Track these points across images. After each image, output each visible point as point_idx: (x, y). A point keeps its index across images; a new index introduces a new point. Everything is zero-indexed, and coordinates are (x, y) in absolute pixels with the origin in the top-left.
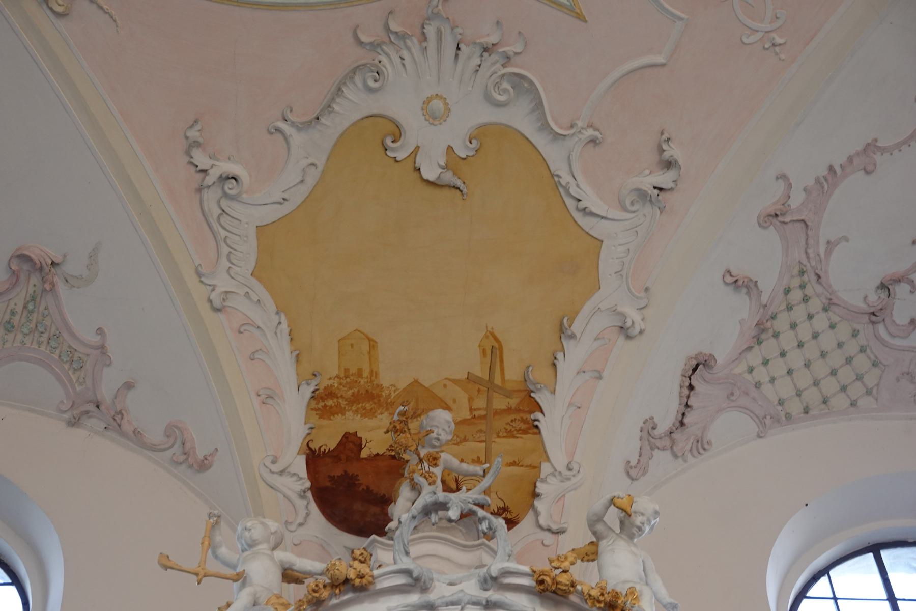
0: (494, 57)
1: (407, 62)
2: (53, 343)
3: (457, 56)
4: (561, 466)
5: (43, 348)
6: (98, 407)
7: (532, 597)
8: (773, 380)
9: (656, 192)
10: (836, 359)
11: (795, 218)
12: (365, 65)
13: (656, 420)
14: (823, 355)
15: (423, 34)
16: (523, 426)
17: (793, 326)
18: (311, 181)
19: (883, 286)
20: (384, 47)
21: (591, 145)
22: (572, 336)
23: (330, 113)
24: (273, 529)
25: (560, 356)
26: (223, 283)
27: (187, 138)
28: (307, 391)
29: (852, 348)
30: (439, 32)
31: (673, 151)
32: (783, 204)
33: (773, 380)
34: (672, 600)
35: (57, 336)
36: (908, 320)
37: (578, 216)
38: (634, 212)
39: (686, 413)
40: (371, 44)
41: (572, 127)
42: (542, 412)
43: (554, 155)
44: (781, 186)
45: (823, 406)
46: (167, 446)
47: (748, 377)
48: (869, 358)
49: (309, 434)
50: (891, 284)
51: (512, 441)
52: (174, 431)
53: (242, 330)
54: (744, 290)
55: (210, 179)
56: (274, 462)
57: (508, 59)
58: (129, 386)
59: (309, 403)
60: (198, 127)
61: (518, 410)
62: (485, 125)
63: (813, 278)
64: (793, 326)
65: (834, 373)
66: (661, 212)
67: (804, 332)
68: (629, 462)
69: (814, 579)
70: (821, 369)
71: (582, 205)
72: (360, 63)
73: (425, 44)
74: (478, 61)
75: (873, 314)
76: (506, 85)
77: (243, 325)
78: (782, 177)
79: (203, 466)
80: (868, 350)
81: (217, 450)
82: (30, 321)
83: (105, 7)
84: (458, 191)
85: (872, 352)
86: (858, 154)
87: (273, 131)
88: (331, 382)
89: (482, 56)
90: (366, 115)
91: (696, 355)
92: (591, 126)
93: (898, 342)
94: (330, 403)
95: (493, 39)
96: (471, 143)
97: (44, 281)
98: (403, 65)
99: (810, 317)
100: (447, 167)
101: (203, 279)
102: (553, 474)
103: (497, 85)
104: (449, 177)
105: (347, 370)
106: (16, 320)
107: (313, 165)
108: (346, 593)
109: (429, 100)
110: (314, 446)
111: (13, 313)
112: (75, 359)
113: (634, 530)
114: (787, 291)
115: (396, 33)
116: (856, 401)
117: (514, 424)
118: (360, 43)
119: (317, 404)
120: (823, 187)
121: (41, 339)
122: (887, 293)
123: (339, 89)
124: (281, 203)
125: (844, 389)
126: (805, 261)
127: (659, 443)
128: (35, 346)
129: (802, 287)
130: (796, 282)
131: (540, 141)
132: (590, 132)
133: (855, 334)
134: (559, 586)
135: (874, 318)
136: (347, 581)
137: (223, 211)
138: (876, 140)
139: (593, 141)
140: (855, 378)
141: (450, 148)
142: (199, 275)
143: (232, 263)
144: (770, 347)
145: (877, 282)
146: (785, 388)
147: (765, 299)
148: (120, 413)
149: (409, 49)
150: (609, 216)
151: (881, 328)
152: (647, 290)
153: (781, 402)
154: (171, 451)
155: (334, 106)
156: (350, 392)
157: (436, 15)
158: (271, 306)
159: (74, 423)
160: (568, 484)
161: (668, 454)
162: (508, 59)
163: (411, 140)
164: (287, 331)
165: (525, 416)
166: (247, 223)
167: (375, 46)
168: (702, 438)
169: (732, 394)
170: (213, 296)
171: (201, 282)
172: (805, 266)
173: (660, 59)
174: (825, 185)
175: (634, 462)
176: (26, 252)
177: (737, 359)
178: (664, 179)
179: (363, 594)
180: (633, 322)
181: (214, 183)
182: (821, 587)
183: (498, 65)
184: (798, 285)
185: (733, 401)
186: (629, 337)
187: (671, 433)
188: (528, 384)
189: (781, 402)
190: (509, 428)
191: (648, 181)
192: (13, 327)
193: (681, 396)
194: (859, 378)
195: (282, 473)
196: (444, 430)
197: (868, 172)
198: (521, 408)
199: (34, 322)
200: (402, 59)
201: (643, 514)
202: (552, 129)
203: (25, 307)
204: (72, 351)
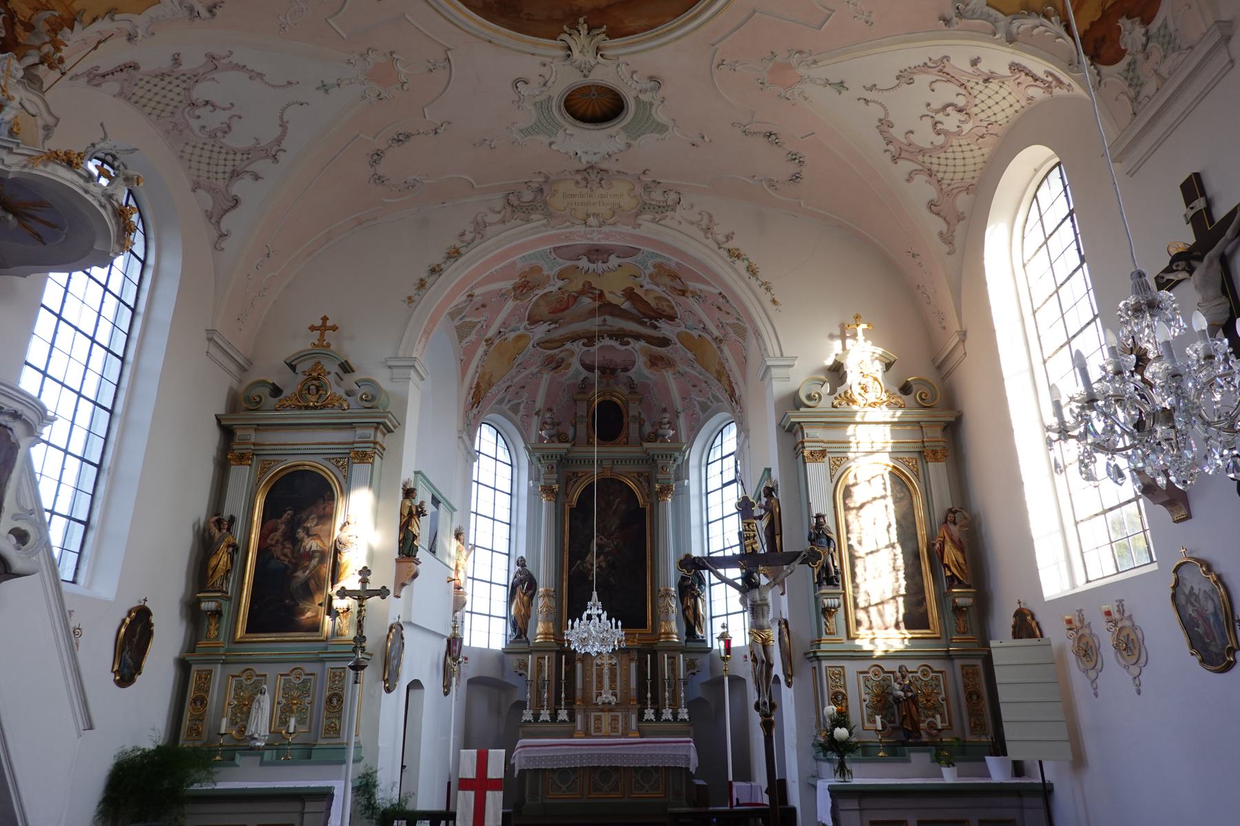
93: (187, 116)
114: (183, 75)
146: (141, 93)
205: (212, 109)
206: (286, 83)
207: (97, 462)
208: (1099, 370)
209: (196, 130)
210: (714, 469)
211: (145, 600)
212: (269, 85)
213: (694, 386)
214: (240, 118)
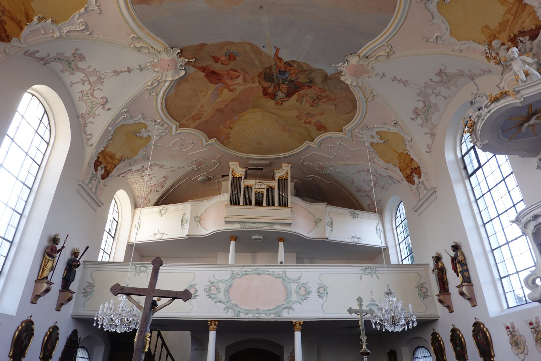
16: (524, 6)
18: (446, 21)
26: (457, 48)
51: (525, 11)
88: (488, 40)
107: (442, 20)
111: (447, 79)
136: (472, 126)
156: (492, 38)
165: (522, 4)
190: (521, 10)
207: (21, 213)
208: (365, 275)
210: (464, 146)
211: (31, 316)
213: (479, 110)
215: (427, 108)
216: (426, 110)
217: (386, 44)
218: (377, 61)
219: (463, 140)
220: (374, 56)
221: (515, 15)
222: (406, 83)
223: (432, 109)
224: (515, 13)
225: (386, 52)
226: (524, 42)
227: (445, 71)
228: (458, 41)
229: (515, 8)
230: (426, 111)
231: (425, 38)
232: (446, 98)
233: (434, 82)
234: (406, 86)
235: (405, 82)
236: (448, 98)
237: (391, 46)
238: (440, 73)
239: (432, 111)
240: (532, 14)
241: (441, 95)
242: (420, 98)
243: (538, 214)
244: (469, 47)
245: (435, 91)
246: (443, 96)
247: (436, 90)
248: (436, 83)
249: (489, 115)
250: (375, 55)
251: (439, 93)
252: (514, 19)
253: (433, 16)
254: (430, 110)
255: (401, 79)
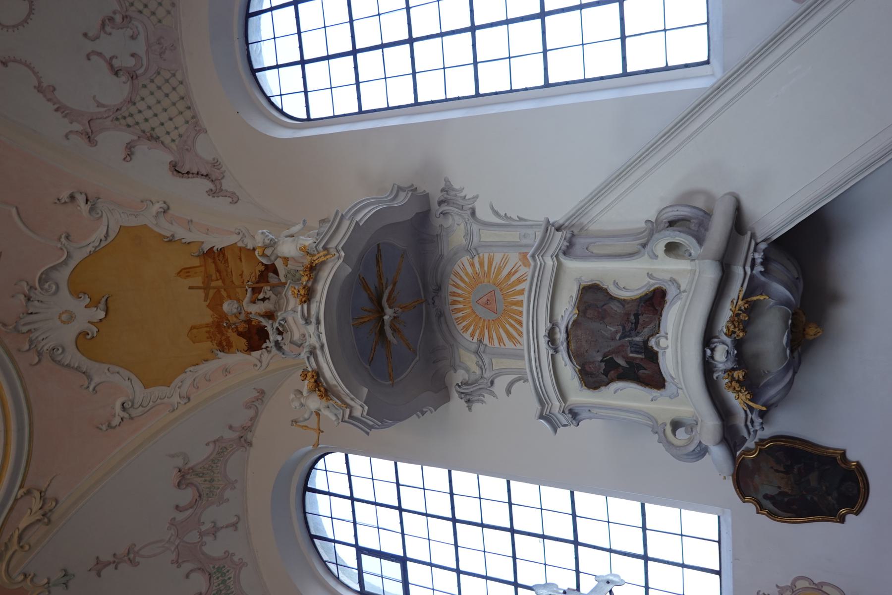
0: (32, 294)
1: (44, 337)
2: (216, 461)
3: (36, 313)
4: (239, 237)
5: (219, 465)
6: (242, 437)
7: (311, 302)
8: (176, 128)
9: (89, 203)
10: (159, 95)
11: (88, 126)
12: (51, 357)
13: (208, 189)
14: (159, 102)
15: (27, 332)
16: (221, 255)
17: (146, 120)
18: (117, 369)
19: (116, 74)
20: (39, 349)
21: (69, 238)
22: (173, 236)
23: (80, 367)
24: (294, 396)
25: (184, 241)
26: (176, 399)
27: (107, 430)
28: (221, 354)
29: (152, 87)
30: (24, 325)
31: (64, 196)
32: (82, 134)
33: (176, 128)
34: (302, 223)
35: (213, 460)
36: (132, 58)
37: (110, 240)
38: (102, 212)
39: (201, 174)
40: (38, 356)
41: (62, 249)
42: (214, 247)
43: (78, 257)
44: (71, 136)
45: (185, 99)
46: (255, 407)
47: (177, 141)
48: (156, 77)
49: (241, 351)
50: (114, 70)
51: (229, 260)
52: (248, 406)
53: (197, 387)
54: (132, 149)
55: (125, 415)
56: (256, 366)
57: (32, 288)
58: (231, 427)
59: (226, 353)
60: (100, 426)
61: (214, 258)
62: (70, 292)
63: (119, 112)
64: (146, 120)
65: (167, 95)
66: (99, 198)
67: (149, 114)
68: (231, 202)
69: (272, 104)
70: (166, 102)
71: (103, 238)
72: (50, 359)
73: (33, 330)
74: (36, 302)
75: (132, 78)
76: (46, 286)
77: (194, 386)
78: (67, 136)
79: (262, 392)
80: (152, 78)
81: (254, 388)
82: (208, 473)
83: (48, 483)
84: (108, 299)
85: (153, 75)
86: (45, 96)
87: (95, 392)
89: (33, 301)
90: (77, 351)
91: (171, 171)
92: (59, 239)
93: (145, 62)
94: (224, 344)
95: (22, 297)
96: (81, 297)
97: (188, 473)
98: (46, 338)
99: (140, 112)
100: (97, 307)
101: (175, 408)
102: (243, 241)
103: (47, 291)
104: (102, 305)
105: (208, 338)
106: (208, 479)
107: (108, 370)
108: (320, 380)
109: (62, 322)
110: (246, 348)
111: (205, 481)
112: (222, 451)
113: (272, 242)
114: (129, 126)
115: (30, 346)
116: (179, 82)
117: (221, 260)
118: (40, 361)
119: (226, 349)
120: (68, 113)
121: (215, 466)
122: (120, 71)
123: (67, 365)
124: (131, 381)
125: (174, 89)
126: (110, 118)
127: (218, 187)
128: (219, 468)
129: (125, 118)
130: (123, 121)
131: (72, 264)
132: (63, 240)
133: (145, 86)
134: (306, 293)
135: (134, 77)
136: (316, 381)
137: (140, 406)
138: (35, 87)
139: (67, 237)
140: (167, 84)
141: (86, 307)
142: (174, 410)
143: (165, 397)
144: (159, 132)
145: (115, 77)
146: (179, 120)
147: (135, 138)
148: (243, 428)
149: (37, 337)
150: (107, 224)
151: (139, 72)
152: (142, 202)
153: (187, 122)
154: (258, 406)
155: (76, 366)
156: (218, 335)
157: (16, 329)
158: (184, 375)
159: (250, 444)
160: (246, 234)
161: (223, 181)
162: (32, 288)
163: (86, 326)
164: (193, 367)
165: (216, 255)
166: (144, 394)
167: (40, 354)
168: (212, 163)
169: (187, 149)
170: (182, 403)
171: (177, 408)
172: (113, 118)
173: (14, 211)
174: (66, 112)
175: (230, 200)
176: (176, 484)
177: (169, 149)
178: (81, 199)
179: (320, 373)
180: (160, 208)
181: (127, 413)
182: (276, 101)
183: (36, 292)
184: (124, 121)
185: (191, 149)
186: (168, 208)
187: (212, 181)
188: (200, 254)
189: (187, 122)
190: (223, 262)
191: (84, 208)
192: (212, 479)
193: (193, 177)
194: (167, 81)
195: (261, 362)
196: (232, 306)
197: (54, 89)
198: (213, 257)
199: (208, 471)
200: (43, 339)
201: (264, 240)
202: (65, 259)
203: (202, 477)
204: (218, 453)
205: (114, 61)
206: (10, 64)
209: (142, 38)
212: (32, 70)
214: (85, 35)
215: (218, 578)
216: (219, 585)
217: (21, 492)
218: (27, 547)
219: (333, 567)
220: (10, 540)
221: (220, 276)
222: (131, 556)
223: (228, 571)
224: (218, 274)
225: (34, 511)
226: (267, 296)
227: (190, 465)
228: (169, 387)
229: (212, 268)
230: (221, 586)
231: (100, 426)
232: (234, 525)
233: (185, 509)
234: (139, 563)
235: (128, 553)
236: (237, 523)
237: (38, 490)
238: (183, 478)
239: (232, 575)
240: (242, 255)
241: (222, 528)
242: (187, 567)
243: (549, 328)
244: (194, 380)
245: (203, 528)
246: (227, 527)
247: (203, 523)
248: (191, 508)
249: (322, 328)
250: (12, 536)
251: (213, 525)
252: (224, 282)
253: (84, 373)
254: (226, 578)
255: (115, 555)
